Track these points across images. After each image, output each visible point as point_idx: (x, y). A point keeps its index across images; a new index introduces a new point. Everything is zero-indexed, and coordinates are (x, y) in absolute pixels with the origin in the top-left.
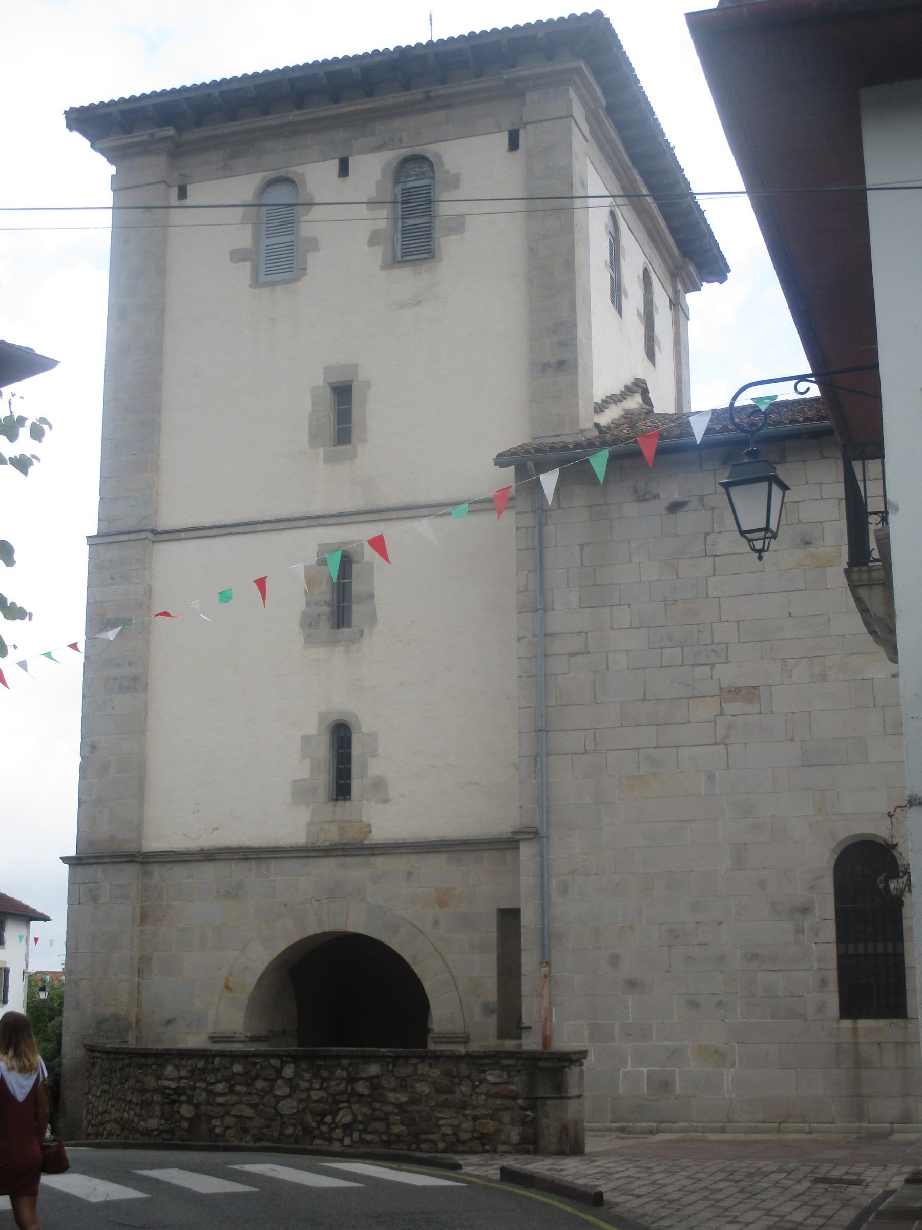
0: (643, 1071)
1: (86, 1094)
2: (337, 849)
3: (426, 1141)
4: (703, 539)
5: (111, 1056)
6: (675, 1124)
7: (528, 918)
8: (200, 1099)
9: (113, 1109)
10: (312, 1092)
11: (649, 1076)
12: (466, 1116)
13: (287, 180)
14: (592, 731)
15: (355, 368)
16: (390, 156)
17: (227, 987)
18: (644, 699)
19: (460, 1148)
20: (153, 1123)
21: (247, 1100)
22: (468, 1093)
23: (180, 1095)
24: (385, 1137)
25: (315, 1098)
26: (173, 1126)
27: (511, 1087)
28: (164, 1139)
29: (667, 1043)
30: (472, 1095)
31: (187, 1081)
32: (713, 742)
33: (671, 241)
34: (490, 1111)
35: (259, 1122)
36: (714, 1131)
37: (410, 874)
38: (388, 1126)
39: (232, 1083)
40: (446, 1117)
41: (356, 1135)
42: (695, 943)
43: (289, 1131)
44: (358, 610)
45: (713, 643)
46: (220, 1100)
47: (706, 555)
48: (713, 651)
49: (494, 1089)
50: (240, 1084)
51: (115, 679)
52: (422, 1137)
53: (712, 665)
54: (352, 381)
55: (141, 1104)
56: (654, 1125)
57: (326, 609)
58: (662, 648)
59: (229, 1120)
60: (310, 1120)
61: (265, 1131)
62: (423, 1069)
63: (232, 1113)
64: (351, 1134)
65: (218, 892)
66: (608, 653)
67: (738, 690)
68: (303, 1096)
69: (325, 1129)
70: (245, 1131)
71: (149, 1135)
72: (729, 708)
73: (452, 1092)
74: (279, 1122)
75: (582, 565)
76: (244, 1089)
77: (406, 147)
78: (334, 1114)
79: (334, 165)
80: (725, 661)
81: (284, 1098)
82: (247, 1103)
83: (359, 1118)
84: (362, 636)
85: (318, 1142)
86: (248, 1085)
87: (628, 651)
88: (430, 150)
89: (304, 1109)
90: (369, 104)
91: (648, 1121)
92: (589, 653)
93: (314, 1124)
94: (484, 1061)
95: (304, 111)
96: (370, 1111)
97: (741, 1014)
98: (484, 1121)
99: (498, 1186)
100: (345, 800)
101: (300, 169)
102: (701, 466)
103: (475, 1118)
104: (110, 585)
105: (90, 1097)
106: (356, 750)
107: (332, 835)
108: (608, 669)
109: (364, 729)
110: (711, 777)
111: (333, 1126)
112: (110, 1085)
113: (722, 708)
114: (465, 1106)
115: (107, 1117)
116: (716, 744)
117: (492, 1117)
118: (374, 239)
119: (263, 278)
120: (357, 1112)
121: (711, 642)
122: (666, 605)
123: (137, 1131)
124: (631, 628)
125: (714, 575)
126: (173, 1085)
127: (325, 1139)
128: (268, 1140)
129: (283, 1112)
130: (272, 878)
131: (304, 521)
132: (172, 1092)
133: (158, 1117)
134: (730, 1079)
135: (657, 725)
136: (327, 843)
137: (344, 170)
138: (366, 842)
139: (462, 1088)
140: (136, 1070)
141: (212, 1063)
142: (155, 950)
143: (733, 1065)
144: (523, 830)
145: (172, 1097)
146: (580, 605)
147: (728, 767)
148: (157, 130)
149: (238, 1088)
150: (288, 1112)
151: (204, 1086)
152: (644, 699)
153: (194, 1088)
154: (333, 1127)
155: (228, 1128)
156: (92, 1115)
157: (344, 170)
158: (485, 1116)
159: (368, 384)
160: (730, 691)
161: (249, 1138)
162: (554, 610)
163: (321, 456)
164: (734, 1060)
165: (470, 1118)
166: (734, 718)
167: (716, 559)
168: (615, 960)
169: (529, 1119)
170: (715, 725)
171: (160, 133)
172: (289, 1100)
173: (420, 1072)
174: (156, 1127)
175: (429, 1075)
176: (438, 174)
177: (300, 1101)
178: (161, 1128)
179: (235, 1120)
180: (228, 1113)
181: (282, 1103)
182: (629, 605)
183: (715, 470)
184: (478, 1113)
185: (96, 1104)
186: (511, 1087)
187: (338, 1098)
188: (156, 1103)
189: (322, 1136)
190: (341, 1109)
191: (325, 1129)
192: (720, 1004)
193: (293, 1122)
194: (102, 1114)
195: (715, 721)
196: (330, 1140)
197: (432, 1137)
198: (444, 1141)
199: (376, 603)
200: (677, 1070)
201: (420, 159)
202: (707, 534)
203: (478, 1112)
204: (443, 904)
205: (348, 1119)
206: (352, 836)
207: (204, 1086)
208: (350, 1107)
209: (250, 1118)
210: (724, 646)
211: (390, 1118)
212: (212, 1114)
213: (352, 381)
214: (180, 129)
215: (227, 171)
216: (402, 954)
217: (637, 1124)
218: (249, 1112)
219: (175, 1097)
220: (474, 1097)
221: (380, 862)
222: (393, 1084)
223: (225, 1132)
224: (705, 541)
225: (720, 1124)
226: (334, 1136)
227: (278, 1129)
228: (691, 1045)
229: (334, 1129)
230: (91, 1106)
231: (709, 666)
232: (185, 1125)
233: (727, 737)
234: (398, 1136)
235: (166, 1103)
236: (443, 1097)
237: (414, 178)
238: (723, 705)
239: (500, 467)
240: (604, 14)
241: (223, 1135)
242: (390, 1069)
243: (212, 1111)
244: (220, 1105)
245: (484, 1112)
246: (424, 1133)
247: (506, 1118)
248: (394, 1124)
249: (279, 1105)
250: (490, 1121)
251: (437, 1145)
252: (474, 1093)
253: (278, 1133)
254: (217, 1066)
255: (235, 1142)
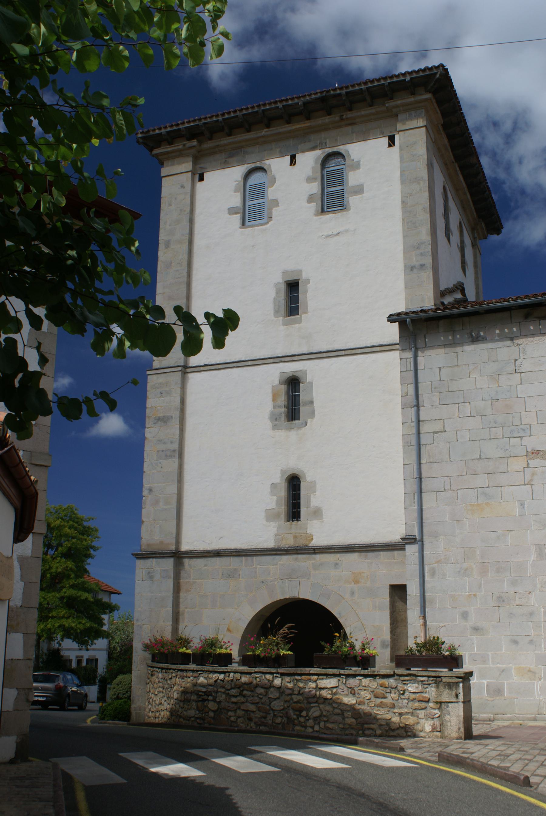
0: (484, 683)
1: (148, 692)
2: (293, 549)
3: (369, 729)
4: (514, 363)
5: (164, 671)
6: (505, 715)
7: (413, 591)
8: (221, 699)
9: (165, 703)
10: (293, 696)
11: (487, 685)
12: (395, 713)
13: (261, 169)
14: (449, 478)
15: (301, 271)
16: (319, 154)
17: (228, 630)
18: (480, 458)
19: (392, 733)
20: (192, 713)
21: (251, 700)
22: (396, 699)
23: (208, 696)
24: (341, 726)
25: (295, 700)
26: (203, 715)
27: (424, 695)
28: (198, 723)
29: (498, 665)
30: (398, 700)
31: (212, 687)
32: (523, 484)
33: (473, 208)
34: (411, 710)
35: (258, 714)
36: (530, 719)
37: (336, 564)
38: (343, 719)
39: (242, 689)
40: (381, 713)
41: (322, 724)
42: (515, 605)
43: (279, 720)
44: (303, 410)
45: (521, 424)
46: (234, 700)
47: (516, 372)
48: (522, 429)
49: (413, 696)
50: (247, 690)
51: (163, 451)
52: (366, 726)
53: (521, 438)
54: (299, 279)
55: (184, 701)
56: (492, 715)
57: (283, 410)
58: (490, 428)
59: (240, 713)
60: (292, 714)
61: (263, 720)
62: (366, 681)
63: (242, 708)
64: (319, 724)
65: (223, 574)
66: (457, 431)
67: (537, 453)
68: (288, 698)
69: (302, 720)
70: (250, 719)
71: (189, 720)
72: (532, 463)
73: (385, 697)
74: (272, 715)
75: (440, 380)
76: (250, 693)
77: (329, 148)
78: (308, 710)
79: (288, 159)
80: (529, 435)
81: (275, 699)
82: (251, 702)
83: (324, 713)
84: (306, 425)
85: (297, 728)
86: (252, 691)
87: (469, 430)
88: (341, 149)
89: (288, 707)
90: (307, 124)
91: (488, 713)
92: (445, 431)
93: (295, 717)
94: (406, 678)
95: (271, 129)
96: (332, 709)
97: (545, 648)
98: (407, 716)
99: (437, 766)
100: (297, 521)
101: (267, 162)
102: (511, 318)
103: (401, 714)
104: (160, 397)
105: (150, 694)
106: (303, 492)
107: (289, 542)
108: (457, 441)
109: (308, 479)
110: (522, 504)
111: (307, 718)
112: (163, 688)
113: (528, 464)
114: (393, 706)
115: (161, 707)
116: (525, 485)
117: (412, 714)
118: (311, 199)
119: (247, 223)
120: (322, 709)
121: (520, 424)
122: (492, 402)
123: (180, 717)
124: (471, 416)
125: (521, 384)
126: (204, 690)
127: (302, 726)
128: (265, 726)
129: (274, 709)
130: (254, 566)
131: (272, 359)
132: (203, 694)
133: (194, 709)
134: (539, 688)
135: (488, 474)
136: (287, 546)
137: (293, 161)
138: (310, 545)
139: (392, 695)
140: (181, 680)
141: (229, 676)
142: (186, 608)
143: (540, 679)
144: (407, 537)
145: (203, 697)
146: (439, 403)
147: (533, 498)
148: (187, 142)
149: (245, 692)
150: (278, 709)
151: (223, 690)
152: (480, 458)
153: (217, 692)
154: (307, 718)
155: (239, 717)
156: (152, 705)
157: (293, 161)
158: (407, 713)
159: (308, 281)
160: (533, 453)
161: (252, 724)
162: (424, 406)
163: (281, 322)
164: (541, 676)
165: (397, 714)
166: (536, 469)
167: (522, 374)
168: (465, 615)
169: (437, 716)
170: (524, 473)
171: (189, 144)
172: (278, 701)
173: (363, 684)
174: (193, 716)
175: (369, 687)
176: (347, 162)
177: (286, 701)
178: (196, 716)
179: (243, 712)
180: (239, 708)
181: (273, 703)
182: (470, 403)
183: (520, 322)
184: (403, 711)
185: (154, 699)
186: (424, 695)
187: (310, 700)
188: (193, 701)
189: (300, 724)
190: (312, 707)
191: (302, 720)
192: (531, 642)
193: (281, 715)
194: (158, 705)
195: (524, 471)
196: (306, 727)
197: (372, 726)
198: (380, 729)
199: (314, 405)
200: (505, 682)
201: (338, 154)
202: (516, 360)
203: (404, 710)
204: (356, 582)
205: (317, 714)
206: (301, 542)
207: (223, 690)
208: (319, 706)
209: (253, 712)
210: (528, 426)
211: (345, 714)
212: (229, 708)
213: (299, 279)
214: (200, 142)
215: (225, 165)
216: (332, 611)
217: (481, 715)
218: (252, 707)
219: (205, 697)
220: (400, 701)
221: (318, 557)
222: (346, 692)
223: (237, 720)
224: (515, 364)
225: (533, 716)
226: (308, 724)
227: (271, 719)
228: (513, 667)
229: (308, 720)
230: (151, 700)
231: (519, 438)
232: (211, 714)
233: (531, 480)
234: (350, 725)
235: (200, 701)
236: (379, 701)
237: (333, 165)
238: (528, 461)
239: (391, 323)
240: (445, 65)
241: (235, 722)
242: (344, 682)
243: (229, 707)
244: (233, 703)
245: (406, 711)
246: (367, 724)
247: (422, 714)
248: (348, 717)
249: (272, 704)
250: (411, 717)
251: (375, 732)
252: (400, 698)
253: (271, 721)
254: (232, 679)
255: (243, 726)
